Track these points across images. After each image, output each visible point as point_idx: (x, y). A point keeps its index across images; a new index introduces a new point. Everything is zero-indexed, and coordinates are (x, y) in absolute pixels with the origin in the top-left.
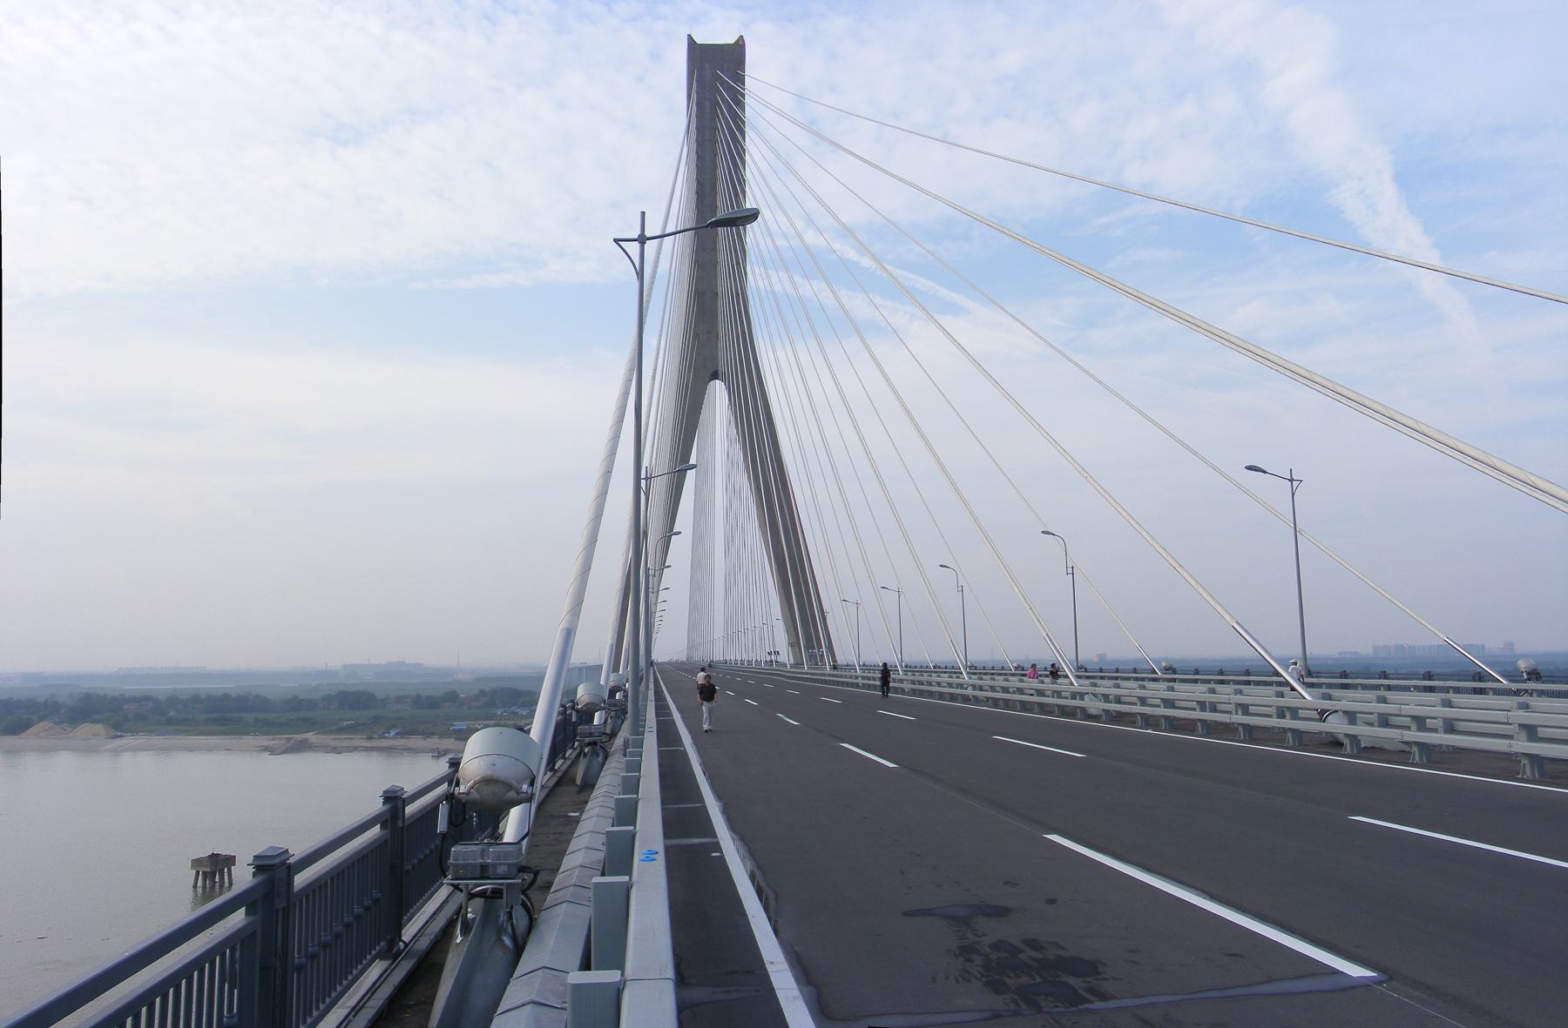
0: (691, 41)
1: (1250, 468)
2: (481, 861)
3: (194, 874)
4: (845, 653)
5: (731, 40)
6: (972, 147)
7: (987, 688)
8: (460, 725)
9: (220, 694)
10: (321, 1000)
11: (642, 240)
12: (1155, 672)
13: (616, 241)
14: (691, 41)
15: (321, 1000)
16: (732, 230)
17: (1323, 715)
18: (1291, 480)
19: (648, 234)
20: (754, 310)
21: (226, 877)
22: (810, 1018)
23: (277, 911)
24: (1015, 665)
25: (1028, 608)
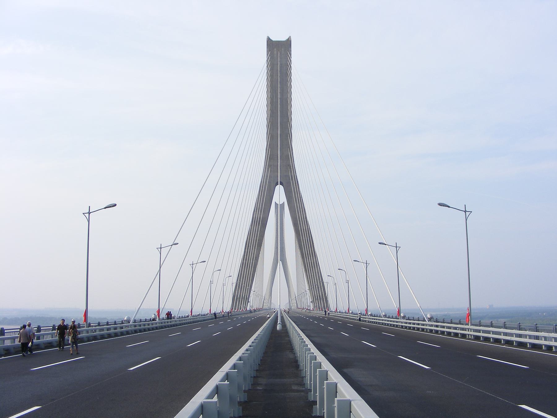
0: (269, 40)
1: (440, 204)
2: (190, 321)
3: (456, 322)
4: (332, 307)
5: (284, 38)
6: (174, 240)
7: (367, 321)
8: (283, 331)
9: (102, 318)
10: (290, 351)
11: (193, 264)
12: (424, 320)
13: (83, 214)
14: (269, 40)
15: (290, 351)
16: (106, 323)
17: (168, 323)
18: (465, 211)
19: (467, 212)
20: (248, 223)
21: (234, 316)
22: (530, 410)
23: (281, 184)
24: (429, 316)
25: (279, 304)
